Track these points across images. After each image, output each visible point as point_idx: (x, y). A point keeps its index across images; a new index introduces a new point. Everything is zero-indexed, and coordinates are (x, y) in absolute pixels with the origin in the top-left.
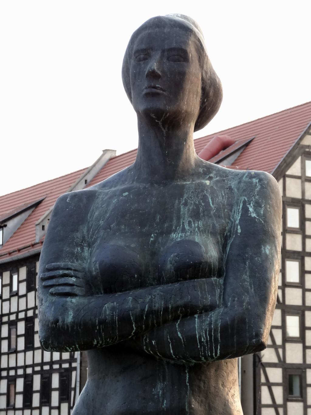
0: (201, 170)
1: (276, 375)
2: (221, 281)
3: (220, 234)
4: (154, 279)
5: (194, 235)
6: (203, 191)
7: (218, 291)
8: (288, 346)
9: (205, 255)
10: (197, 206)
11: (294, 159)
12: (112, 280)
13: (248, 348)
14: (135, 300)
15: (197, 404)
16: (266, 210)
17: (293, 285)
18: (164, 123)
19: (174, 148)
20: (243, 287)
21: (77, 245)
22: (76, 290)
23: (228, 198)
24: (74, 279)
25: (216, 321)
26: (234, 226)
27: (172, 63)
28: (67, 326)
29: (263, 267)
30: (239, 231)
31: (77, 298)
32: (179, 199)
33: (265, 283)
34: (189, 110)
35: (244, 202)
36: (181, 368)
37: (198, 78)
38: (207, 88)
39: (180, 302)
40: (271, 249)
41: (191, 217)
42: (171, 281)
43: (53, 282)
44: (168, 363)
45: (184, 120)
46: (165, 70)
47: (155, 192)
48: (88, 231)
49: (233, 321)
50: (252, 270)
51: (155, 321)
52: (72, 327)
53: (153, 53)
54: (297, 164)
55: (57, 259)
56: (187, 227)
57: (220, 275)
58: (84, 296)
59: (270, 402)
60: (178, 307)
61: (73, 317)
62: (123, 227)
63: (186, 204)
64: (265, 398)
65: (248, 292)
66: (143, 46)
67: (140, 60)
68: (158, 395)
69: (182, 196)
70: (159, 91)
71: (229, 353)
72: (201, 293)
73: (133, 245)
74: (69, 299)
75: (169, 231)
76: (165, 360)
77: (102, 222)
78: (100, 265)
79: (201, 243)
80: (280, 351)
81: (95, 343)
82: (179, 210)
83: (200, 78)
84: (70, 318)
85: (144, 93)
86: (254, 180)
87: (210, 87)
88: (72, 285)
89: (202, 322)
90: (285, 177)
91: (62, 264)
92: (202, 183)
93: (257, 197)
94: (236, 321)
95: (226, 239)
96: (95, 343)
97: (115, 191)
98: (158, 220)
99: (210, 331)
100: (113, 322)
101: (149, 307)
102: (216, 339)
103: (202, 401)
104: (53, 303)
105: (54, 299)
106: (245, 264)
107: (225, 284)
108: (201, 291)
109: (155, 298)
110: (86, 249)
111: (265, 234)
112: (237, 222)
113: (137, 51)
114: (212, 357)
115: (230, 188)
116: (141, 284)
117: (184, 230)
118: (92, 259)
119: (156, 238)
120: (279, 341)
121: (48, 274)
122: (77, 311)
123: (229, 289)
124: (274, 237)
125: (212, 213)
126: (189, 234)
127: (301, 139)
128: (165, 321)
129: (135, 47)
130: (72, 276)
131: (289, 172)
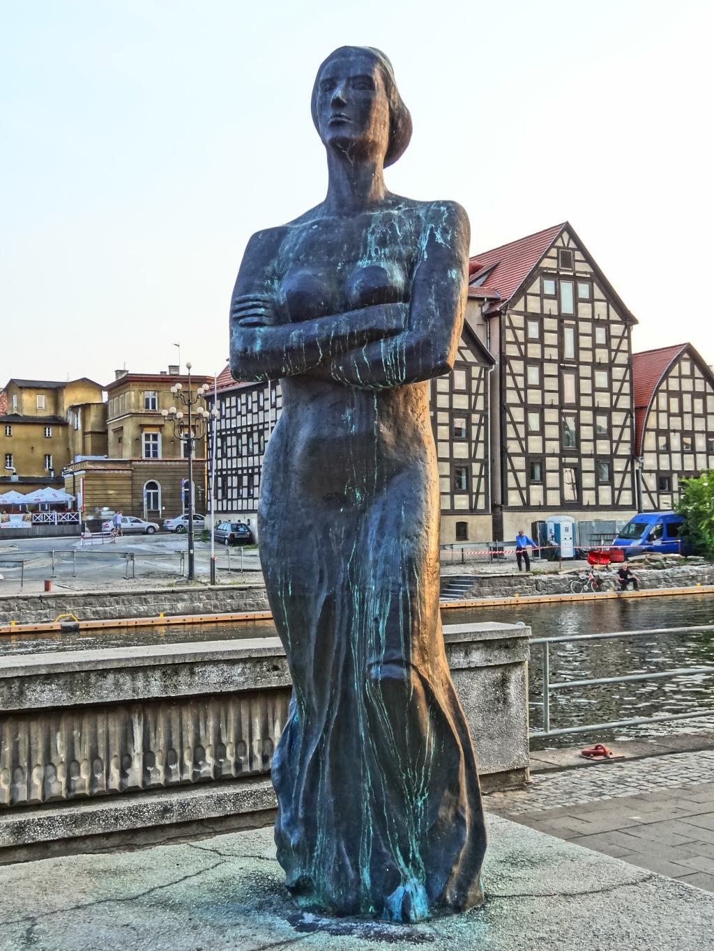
0: (390, 202)
1: (520, 463)
2: (407, 306)
3: (406, 260)
4: (341, 306)
5: (380, 260)
6: (390, 220)
7: (403, 315)
8: (530, 438)
9: (390, 280)
10: (384, 234)
11: (534, 280)
12: (299, 308)
13: (433, 370)
14: (321, 326)
15: (386, 429)
16: (453, 237)
17: (533, 387)
18: (351, 153)
19: (362, 179)
20: (428, 310)
21: (268, 278)
22: (265, 320)
23: (416, 226)
24: (263, 310)
25: (401, 344)
26: (420, 251)
27: (357, 91)
28: (256, 356)
29: (449, 290)
30: (426, 257)
31: (266, 328)
32: (367, 229)
33: (451, 307)
34: (377, 140)
35: (432, 229)
36: (369, 394)
37: (385, 108)
38: (396, 118)
39: (365, 327)
40: (458, 274)
41: (378, 245)
42: (357, 306)
43: (243, 313)
44: (356, 389)
45: (372, 150)
46: (355, 104)
47: (343, 223)
48: (279, 265)
49: (418, 343)
50: (438, 294)
51: (341, 346)
52: (261, 355)
53: (338, 82)
54: (537, 282)
55: (247, 292)
56: (373, 255)
57: (405, 301)
58: (272, 325)
59: (515, 485)
60: (363, 332)
61: (262, 346)
62: (311, 258)
63: (373, 233)
64: (511, 482)
65: (433, 315)
66: (329, 76)
67: (326, 91)
68: (347, 420)
69: (370, 225)
70: (344, 119)
71: (416, 376)
72: (387, 317)
73: (320, 274)
74: (257, 329)
75: (357, 259)
76: (353, 387)
77: (291, 255)
78: (287, 294)
79: (386, 269)
80: (523, 443)
81: (284, 371)
82: (366, 238)
83: (388, 107)
84: (258, 347)
85: (329, 123)
86: (443, 208)
87: (398, 118)
88: (260, 315)
89: (387, 346)
90: (526, 295)
91: (251, 296)
92: (390, 213)
93: (444, 224)
94: (421, 344)
95: (413, 265)
96: (284, 371)
97: (305, 226)
98: (345, 249)
99: (395, 355)
100: (300, 349)
101: (335, 332)
102: (401, 362)
103: (390, 426)
104: (242, 333)
105: (243, 329)
106: (431, 288)
107: (411, 308)
108: (384, 316)
109: (341, 324)
110: (276, 281)
111: (451, 259)
112: (424, 248)
113: (324, 82)
114: (398, 380)
115: (418, 217)
116: (329, 311)
117: (370, 257)
118: (281, 292)
119: (343, 267)
120: (522, 435)
121: (238, 306)
122: (265, 339)
123: (414, 314)
124: (461, 262)
125: (399, 240)
126: (374, 260)
127: (540, 262)
128: (352, 347)
129: (321, 78)
130: (260, 307)
131: (529, 291)
